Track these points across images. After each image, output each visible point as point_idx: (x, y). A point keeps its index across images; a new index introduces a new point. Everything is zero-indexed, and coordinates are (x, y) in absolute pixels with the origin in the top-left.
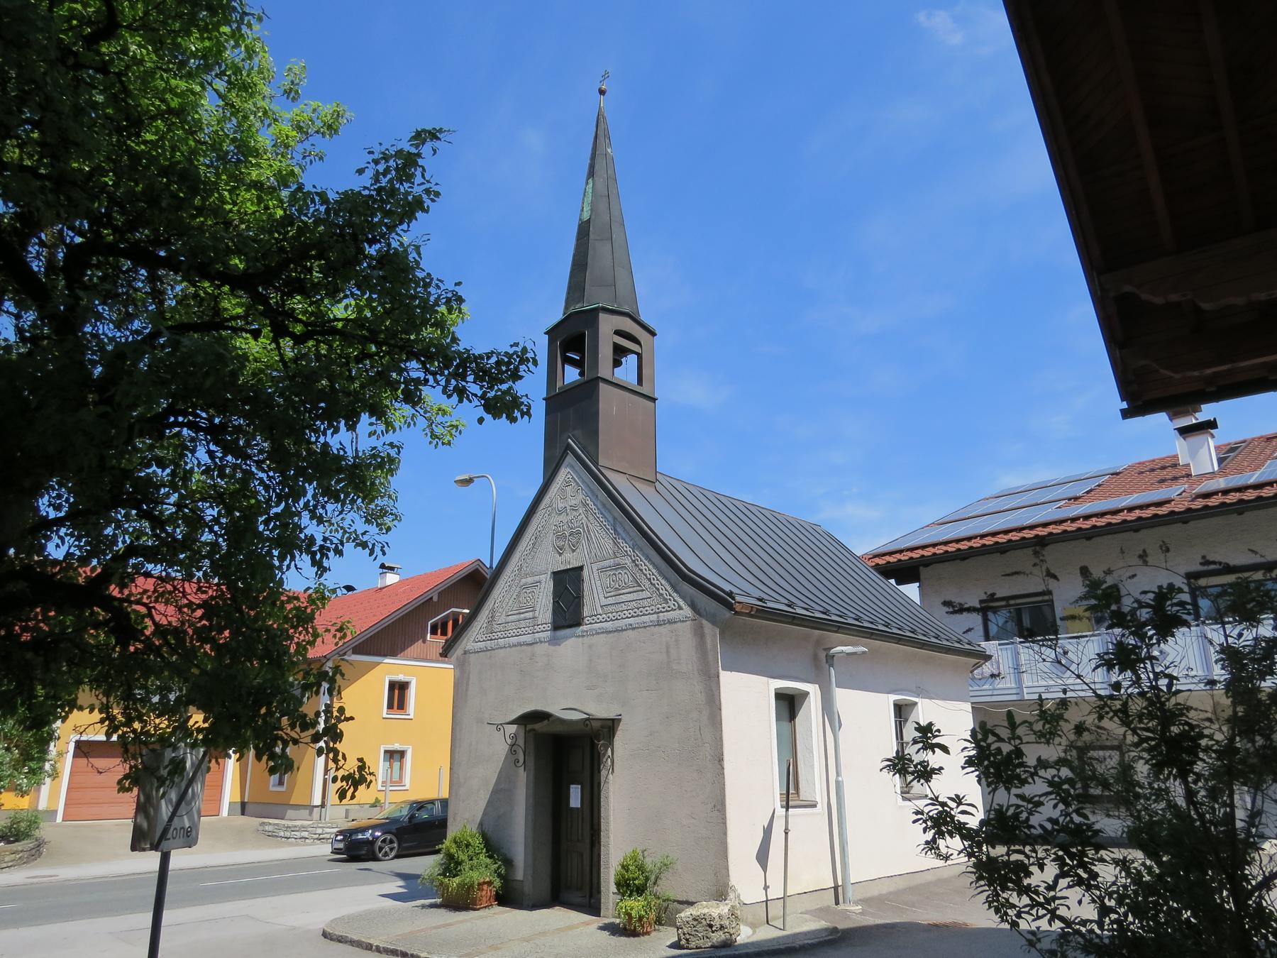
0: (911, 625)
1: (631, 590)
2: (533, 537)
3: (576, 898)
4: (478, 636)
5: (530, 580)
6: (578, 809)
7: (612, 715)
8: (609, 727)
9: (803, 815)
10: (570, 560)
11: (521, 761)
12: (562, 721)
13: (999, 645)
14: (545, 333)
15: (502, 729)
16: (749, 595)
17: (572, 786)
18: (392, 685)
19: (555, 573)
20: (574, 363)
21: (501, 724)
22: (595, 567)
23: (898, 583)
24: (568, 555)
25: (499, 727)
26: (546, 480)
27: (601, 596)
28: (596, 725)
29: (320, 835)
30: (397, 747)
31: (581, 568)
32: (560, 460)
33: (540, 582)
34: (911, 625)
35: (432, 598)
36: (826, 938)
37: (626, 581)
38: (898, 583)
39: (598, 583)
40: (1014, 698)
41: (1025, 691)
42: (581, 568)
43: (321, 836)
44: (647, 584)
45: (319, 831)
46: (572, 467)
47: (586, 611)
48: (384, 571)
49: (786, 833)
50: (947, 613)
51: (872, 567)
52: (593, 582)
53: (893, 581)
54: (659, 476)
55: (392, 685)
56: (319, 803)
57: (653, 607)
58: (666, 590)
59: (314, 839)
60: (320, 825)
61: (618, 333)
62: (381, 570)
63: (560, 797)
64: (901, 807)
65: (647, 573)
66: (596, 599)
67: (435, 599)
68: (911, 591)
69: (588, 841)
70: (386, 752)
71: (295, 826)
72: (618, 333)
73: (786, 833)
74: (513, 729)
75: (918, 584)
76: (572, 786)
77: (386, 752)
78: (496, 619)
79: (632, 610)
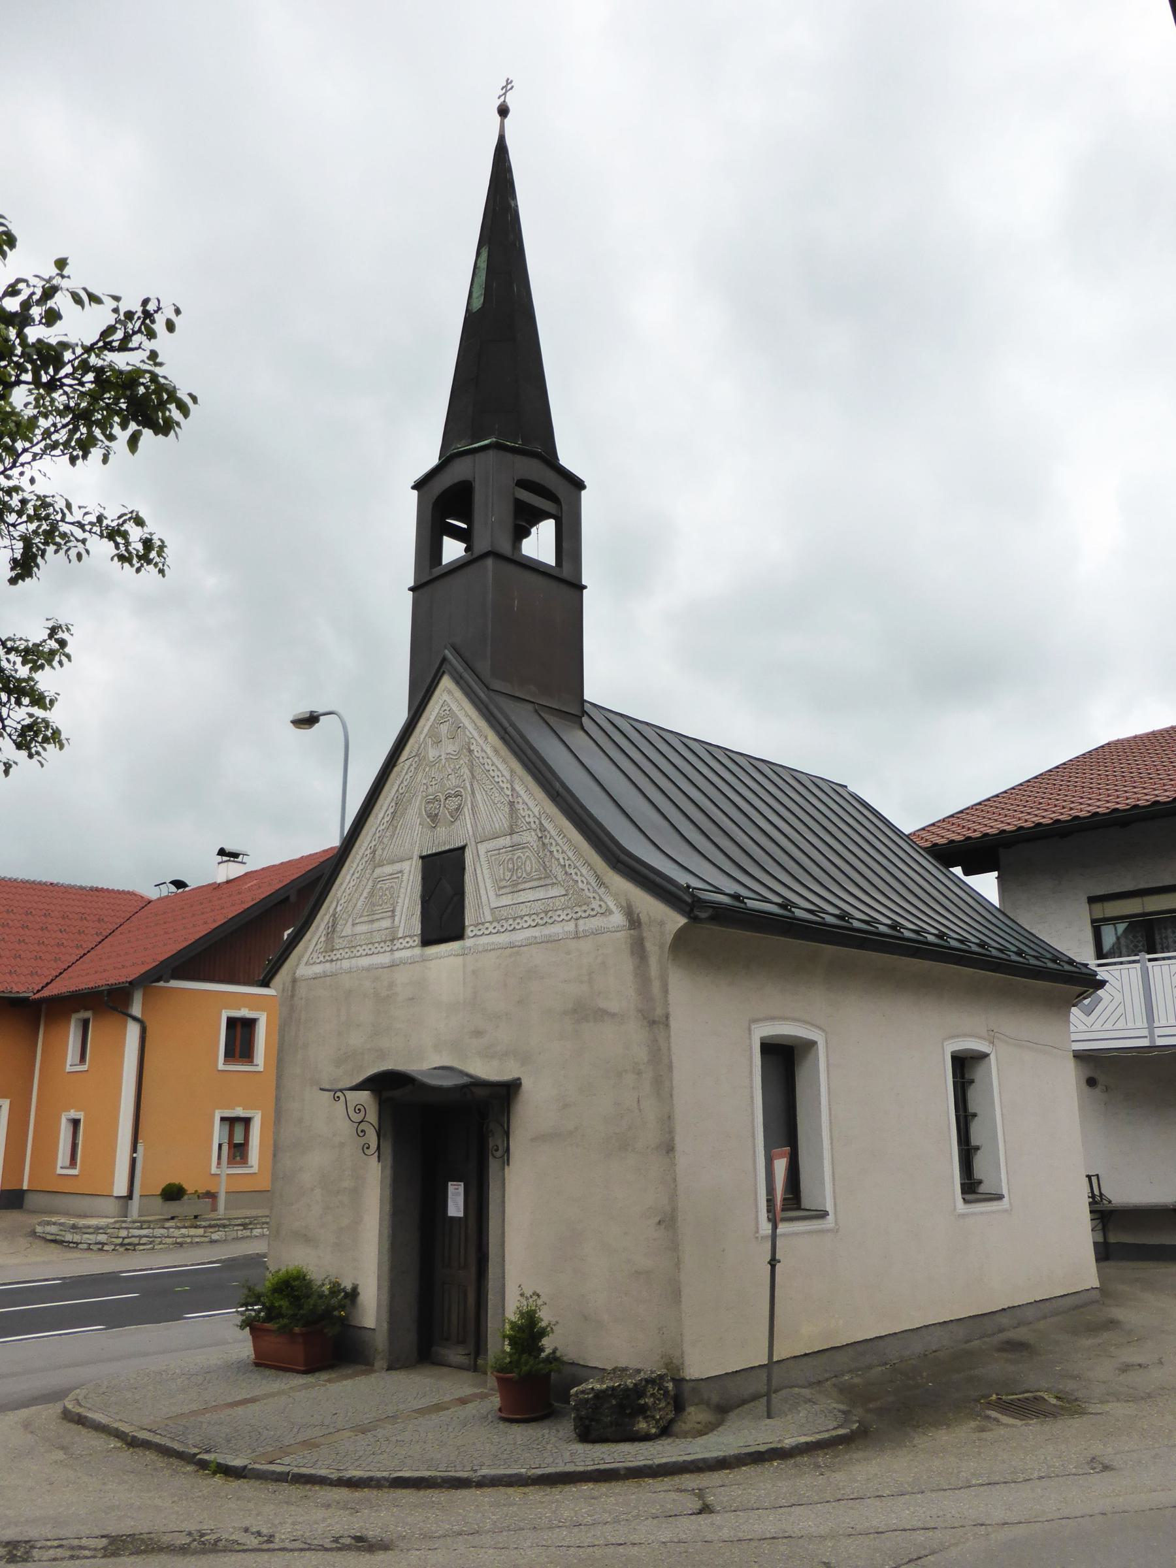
0: (1017, 943)
1: (535, 884)
2: (393, 804)
3: (456, 1355)
4: (315, 955)
5: (388, 869)
6: (460, 1218)
7: (506, 1077)
8: (508, 1091)
9: (810, 1232)
10: (443, 841)
11: (374, 1146)
12: (439, 1089)
13: (1150, 960)
14: (414, 488)
15: (342, 1098)
16: (719, 891)
17: (450, 1183)
18: (232, 1023)
19: (422, 858)
20: (457, 534)
21: (341, 1090)
22: (482, 848)
23: (966, 873)
24: (442, 831)
25: (336, 1093)
26: (412, 712)
27: (492, 894)
28: (480, 1092)
29: (124, 1238)
30: (240, 1112)
31: (463, 848)
32: (432, 682)
33: (401, 872)
34: (1017, 943)
35: (287, 898)
36: (834, 1433)
37: (528, 869)
38: (966, 873)
39: (486, 872)
40: (1145, 1043)
41: (1158, 1032)
42: (463, 848)
43: (127, 1241)
44: (561, 876)
45: (124, 1233)
46: (450, 692)
47: (469, 918)
48: (225, 858)
49: (773, 1267)
50: (180, 428)
51: (925, 849)
52: (479, 872)
53: (958, 871)
54: (587, 707)
55: (232, 1023)
56: (125, 1194)
57: (569, 911)
58: (588, 883)
59: (116, 1245)
60: (124, 1225)
61: (523, 484)
62: (219, 858)
63: (435, 1200)
64: (963, 1216)
65: (560, 856)
66: (484, 898)
67: (293, 899)
68: (986, 885)
69: (473, 1269)
70: (223, 1119)
71: (89, 1227)
72: (523, 484)
73: (773, 1267)
74: (364, 1096)
75: (996, 874)
76: (450, 1183)
77: (223, 1119)
78: (339, 928)
79: (537, 914)
